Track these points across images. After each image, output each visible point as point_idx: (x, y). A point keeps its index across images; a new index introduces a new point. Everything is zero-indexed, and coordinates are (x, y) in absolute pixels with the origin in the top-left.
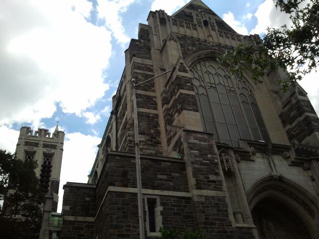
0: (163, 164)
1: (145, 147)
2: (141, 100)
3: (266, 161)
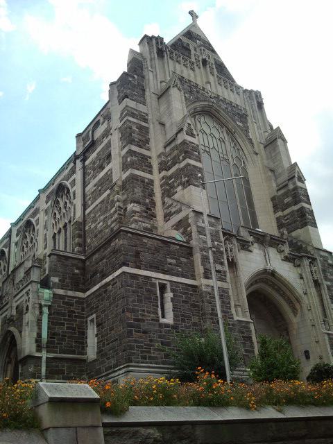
0: (173, 248)
1: (140, 219)
2: (136, 159)
3: (262, 252)
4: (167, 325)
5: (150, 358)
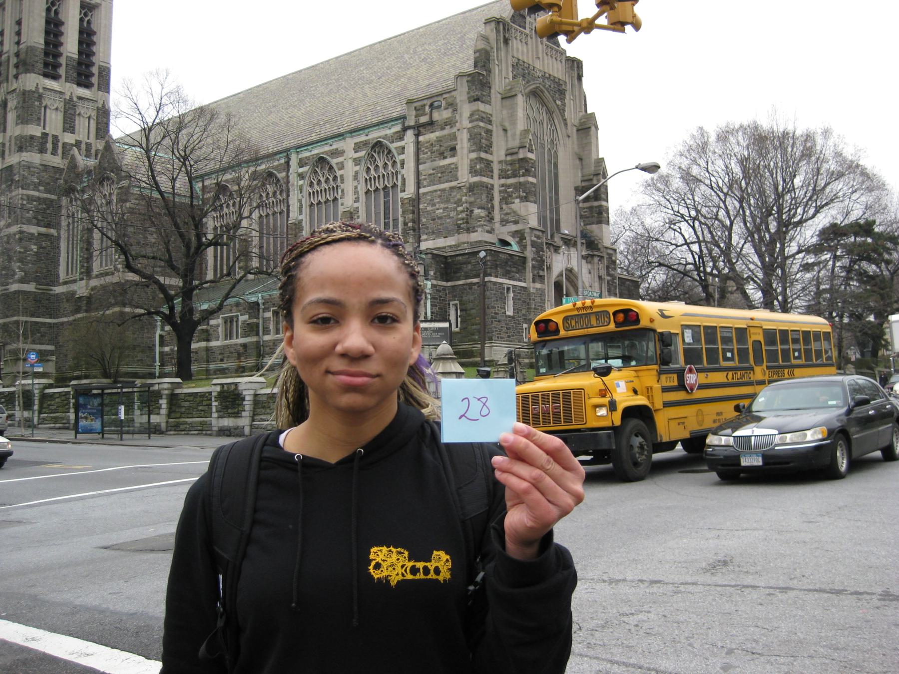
4: (509, 317)
5: (501, 338)
